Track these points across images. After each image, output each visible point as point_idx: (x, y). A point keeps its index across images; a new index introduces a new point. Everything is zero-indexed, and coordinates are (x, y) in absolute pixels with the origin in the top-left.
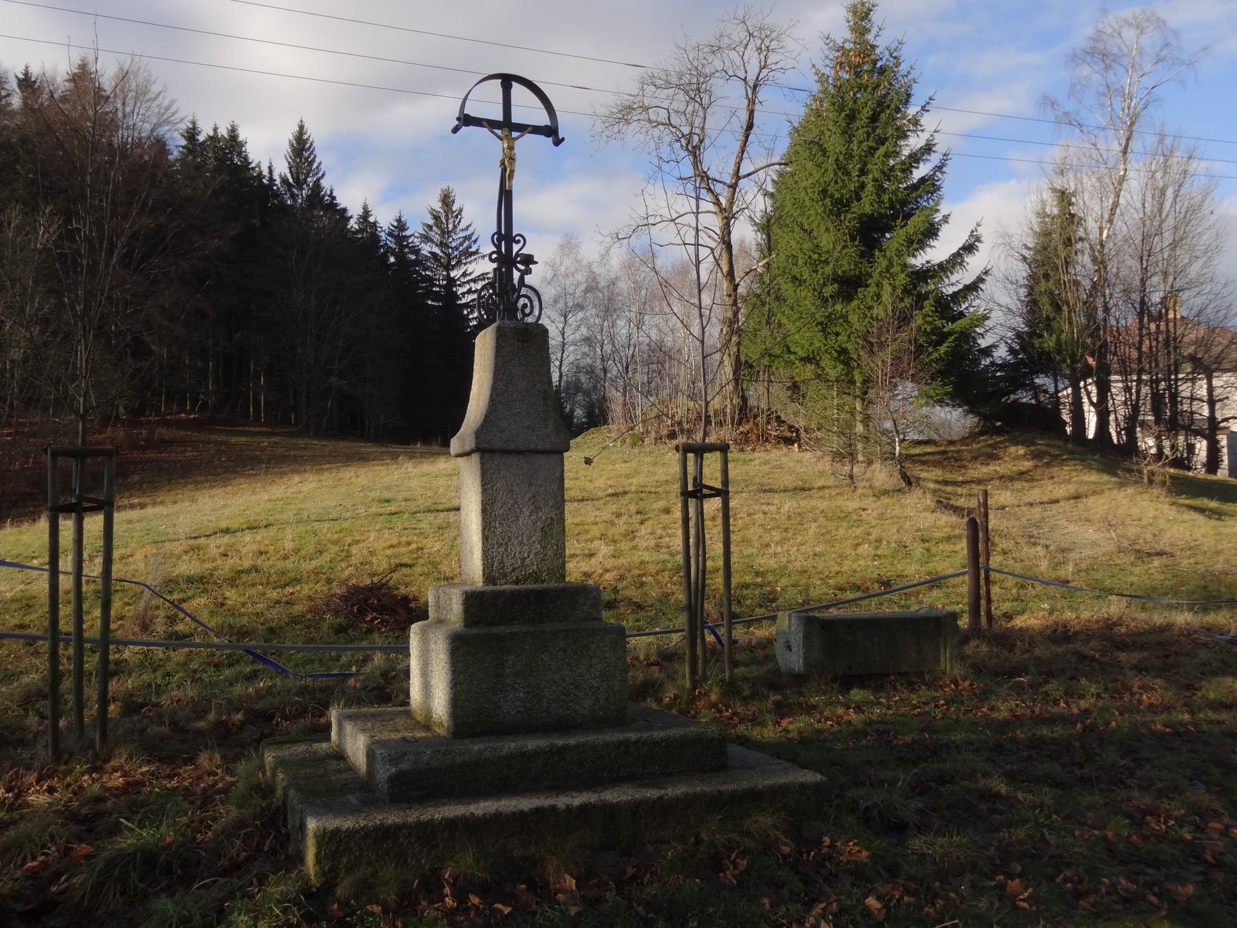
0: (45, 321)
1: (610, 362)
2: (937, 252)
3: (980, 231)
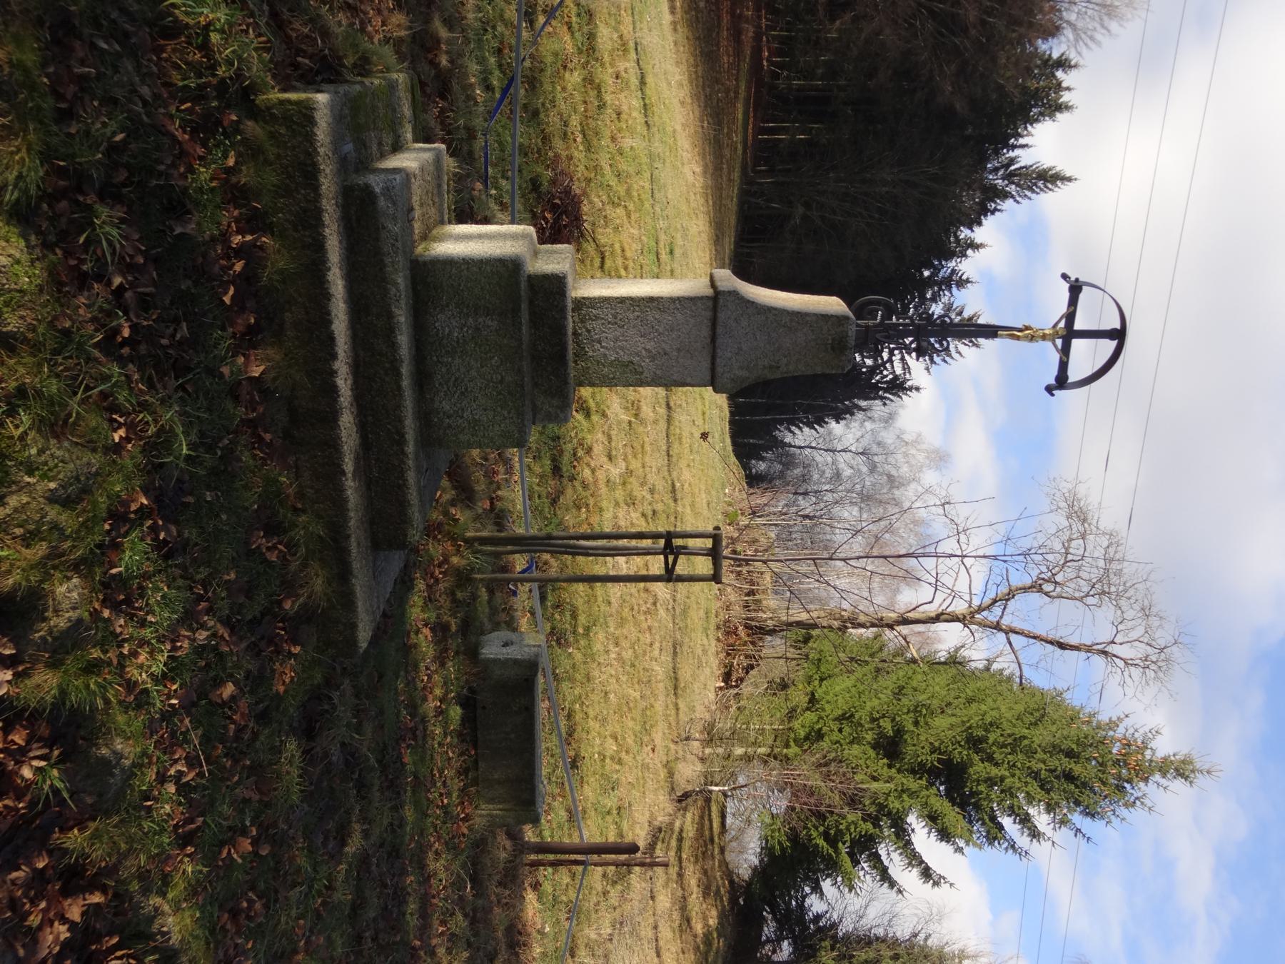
1: (814, 499)
2: (923, 838)
3: (945, 887)
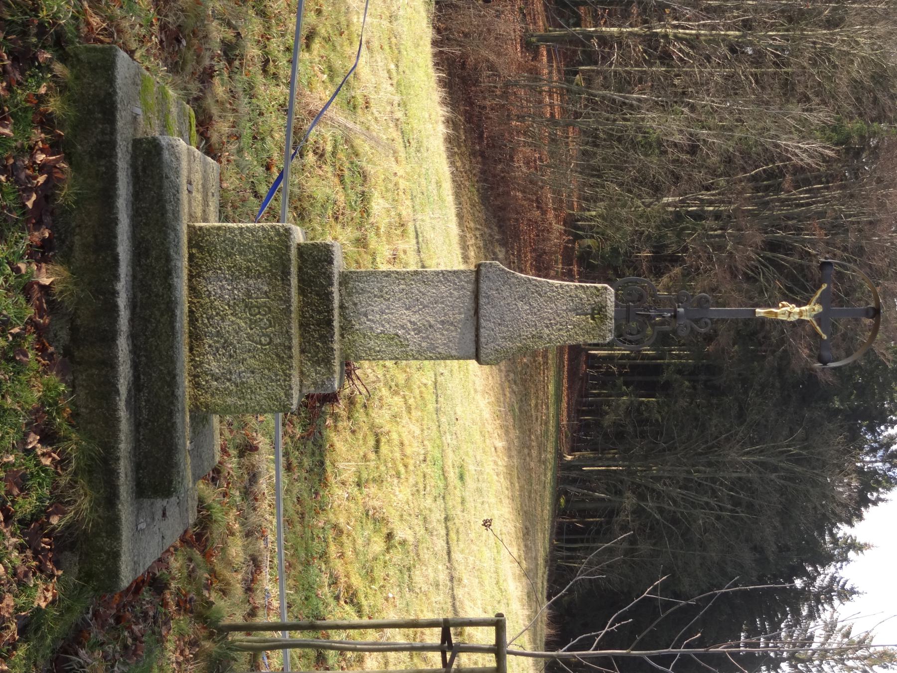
0: (693, 149)
